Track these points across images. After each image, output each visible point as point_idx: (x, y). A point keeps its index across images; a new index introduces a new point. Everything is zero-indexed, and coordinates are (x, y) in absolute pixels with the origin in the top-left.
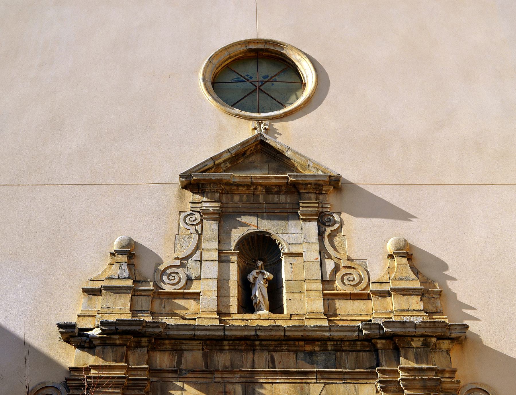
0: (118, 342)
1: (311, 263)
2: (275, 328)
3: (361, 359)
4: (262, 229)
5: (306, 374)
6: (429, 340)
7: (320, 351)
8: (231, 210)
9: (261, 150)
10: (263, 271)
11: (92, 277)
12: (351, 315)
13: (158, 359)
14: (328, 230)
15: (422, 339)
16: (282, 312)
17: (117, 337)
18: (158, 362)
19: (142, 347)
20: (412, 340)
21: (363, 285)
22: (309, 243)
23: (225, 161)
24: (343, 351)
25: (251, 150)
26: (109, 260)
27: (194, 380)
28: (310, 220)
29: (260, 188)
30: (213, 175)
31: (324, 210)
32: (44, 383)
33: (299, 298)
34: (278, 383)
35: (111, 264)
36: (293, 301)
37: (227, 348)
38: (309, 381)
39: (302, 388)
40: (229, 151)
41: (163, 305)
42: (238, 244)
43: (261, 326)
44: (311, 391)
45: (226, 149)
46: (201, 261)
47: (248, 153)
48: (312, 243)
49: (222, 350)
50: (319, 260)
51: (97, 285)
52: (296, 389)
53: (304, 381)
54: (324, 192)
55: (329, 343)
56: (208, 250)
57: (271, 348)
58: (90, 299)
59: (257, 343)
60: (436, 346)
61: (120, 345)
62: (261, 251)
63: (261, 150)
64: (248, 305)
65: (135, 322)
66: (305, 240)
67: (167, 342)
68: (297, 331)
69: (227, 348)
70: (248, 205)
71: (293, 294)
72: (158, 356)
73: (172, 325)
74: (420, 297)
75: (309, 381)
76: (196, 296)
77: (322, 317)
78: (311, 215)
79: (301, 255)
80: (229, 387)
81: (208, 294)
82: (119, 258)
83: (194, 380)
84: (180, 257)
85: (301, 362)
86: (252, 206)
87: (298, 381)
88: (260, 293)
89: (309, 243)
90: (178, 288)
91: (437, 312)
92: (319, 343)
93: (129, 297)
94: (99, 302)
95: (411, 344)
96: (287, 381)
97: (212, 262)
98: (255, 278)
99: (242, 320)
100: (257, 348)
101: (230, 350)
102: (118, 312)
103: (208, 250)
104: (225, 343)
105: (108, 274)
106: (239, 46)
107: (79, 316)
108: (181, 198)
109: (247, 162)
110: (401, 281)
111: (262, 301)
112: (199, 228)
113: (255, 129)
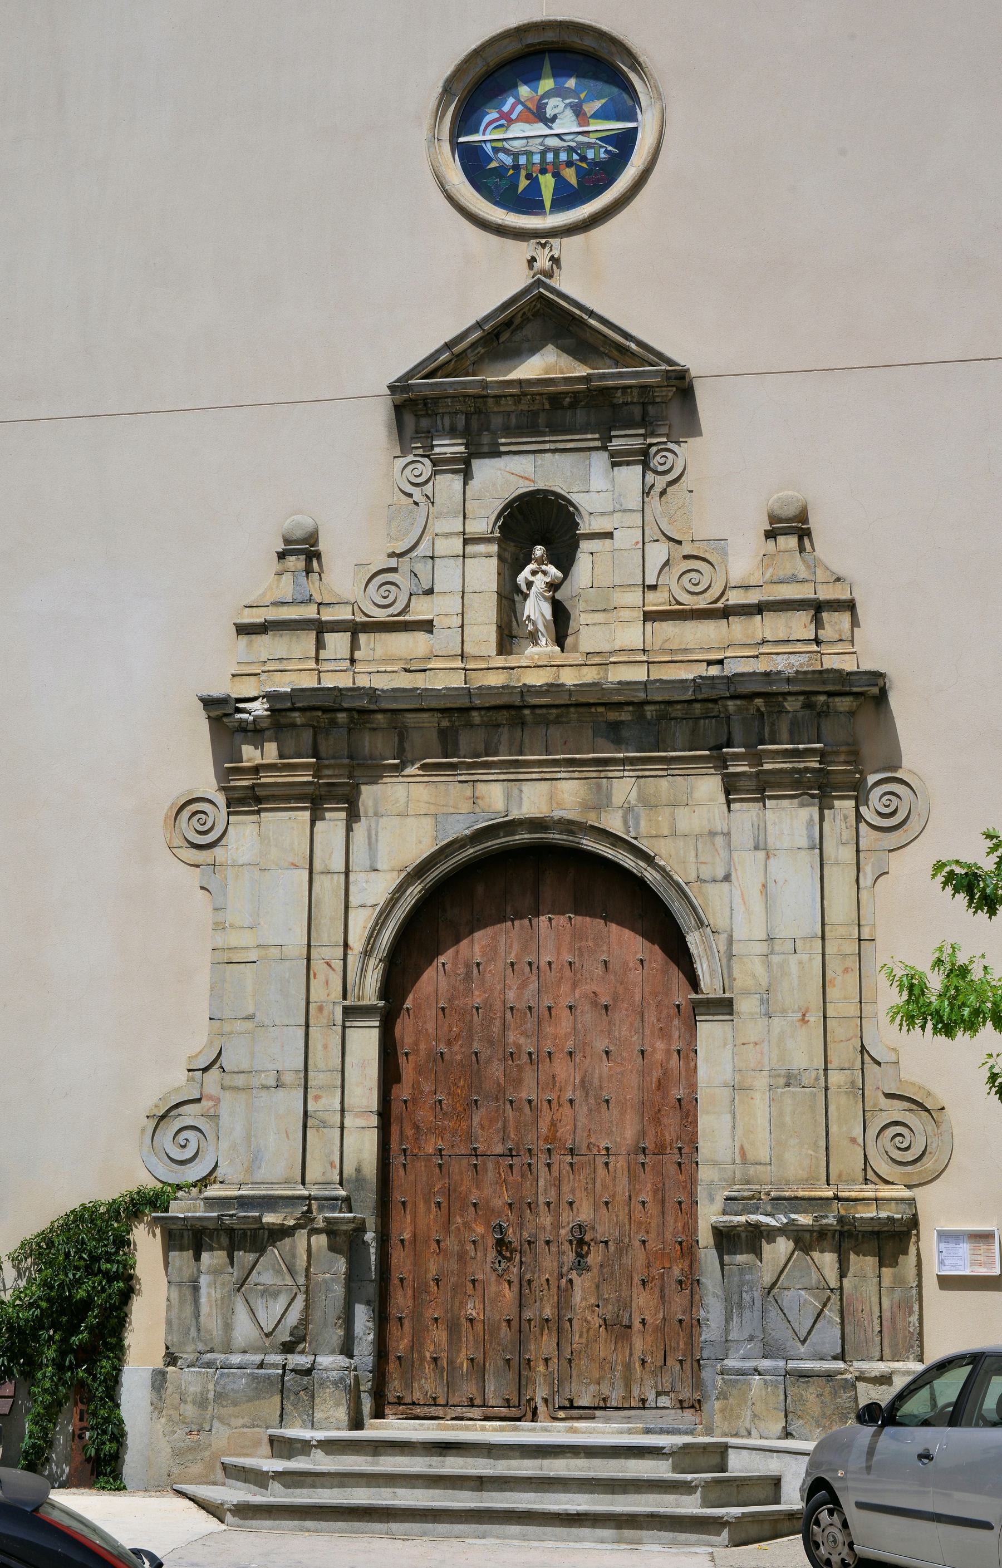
1: (626, 553)
2: (553, 689)
3: (702, 730)
4: (541, 485)
5: (606, 762)
6: (814, 699)
9: (541, 316)
10: (544, 567)
11: (248, 602)
12: (685, 651)
13: (367, 744)
15: (801, 698)
17: (296, 714)
18: (367, 749)
20: (785, 700)
21: (715, 592)
22: (624, 511)
23: (473, 345)
24: (671, 719)
25: (524, 313)
26: (275, 565)
27: (426, 779)
28: (628, 463)
32: (190, 792)
33: (603, 621)
34: (560, 779)
35: (279, 574)
36: (591, 627)
38: (610, 774)
39: (599, 787)
40: (479, 325)
41: (372, 646)
42: (584, 361)
43: (530, 686)
44: (614, 791)
45: (473, 322)
46: (432, 558)
47: (517, 321)
48: (630, 511)
50: (640, 545)
51: (256, 617)
52: (590, 789)
53: (603, 774)
54: (658, 400)
55: (648, 708)
56: (447, 535)
58: (250, 644)
59: (527, 712)
60: (828, 707)
62: (539, 527)
63: (541, 316)
64: (509, 635)
65: (321, 693)
71: (592, 615)
72: (367, 739)
73: (382, 690)
74: (812, 612)
75: (610, 774)
76: (427, 626)
77: (638, 659)
79: (609, 535)
81: (447, 622)
82: (291, 564)
84: (397, 552)
85: (600, 741)
87: (594, 775)
88: (536, 609)
89: (624, 511)
90: (396, 613)
91: (841, 640)
92: (631, 708)
93: (313, 635)
94: (266, 646)
95: (784, 707)
96: (576, 775)
97: (452, 560)
99: (503, 668)
102: (296, 668)
103: (447, 535)
104: (475, 714)
105: (278, 595)
106: (506, 42)
107: (233, 676)
109: (518, 337)
110: (781, 585)
112: (428, 489)
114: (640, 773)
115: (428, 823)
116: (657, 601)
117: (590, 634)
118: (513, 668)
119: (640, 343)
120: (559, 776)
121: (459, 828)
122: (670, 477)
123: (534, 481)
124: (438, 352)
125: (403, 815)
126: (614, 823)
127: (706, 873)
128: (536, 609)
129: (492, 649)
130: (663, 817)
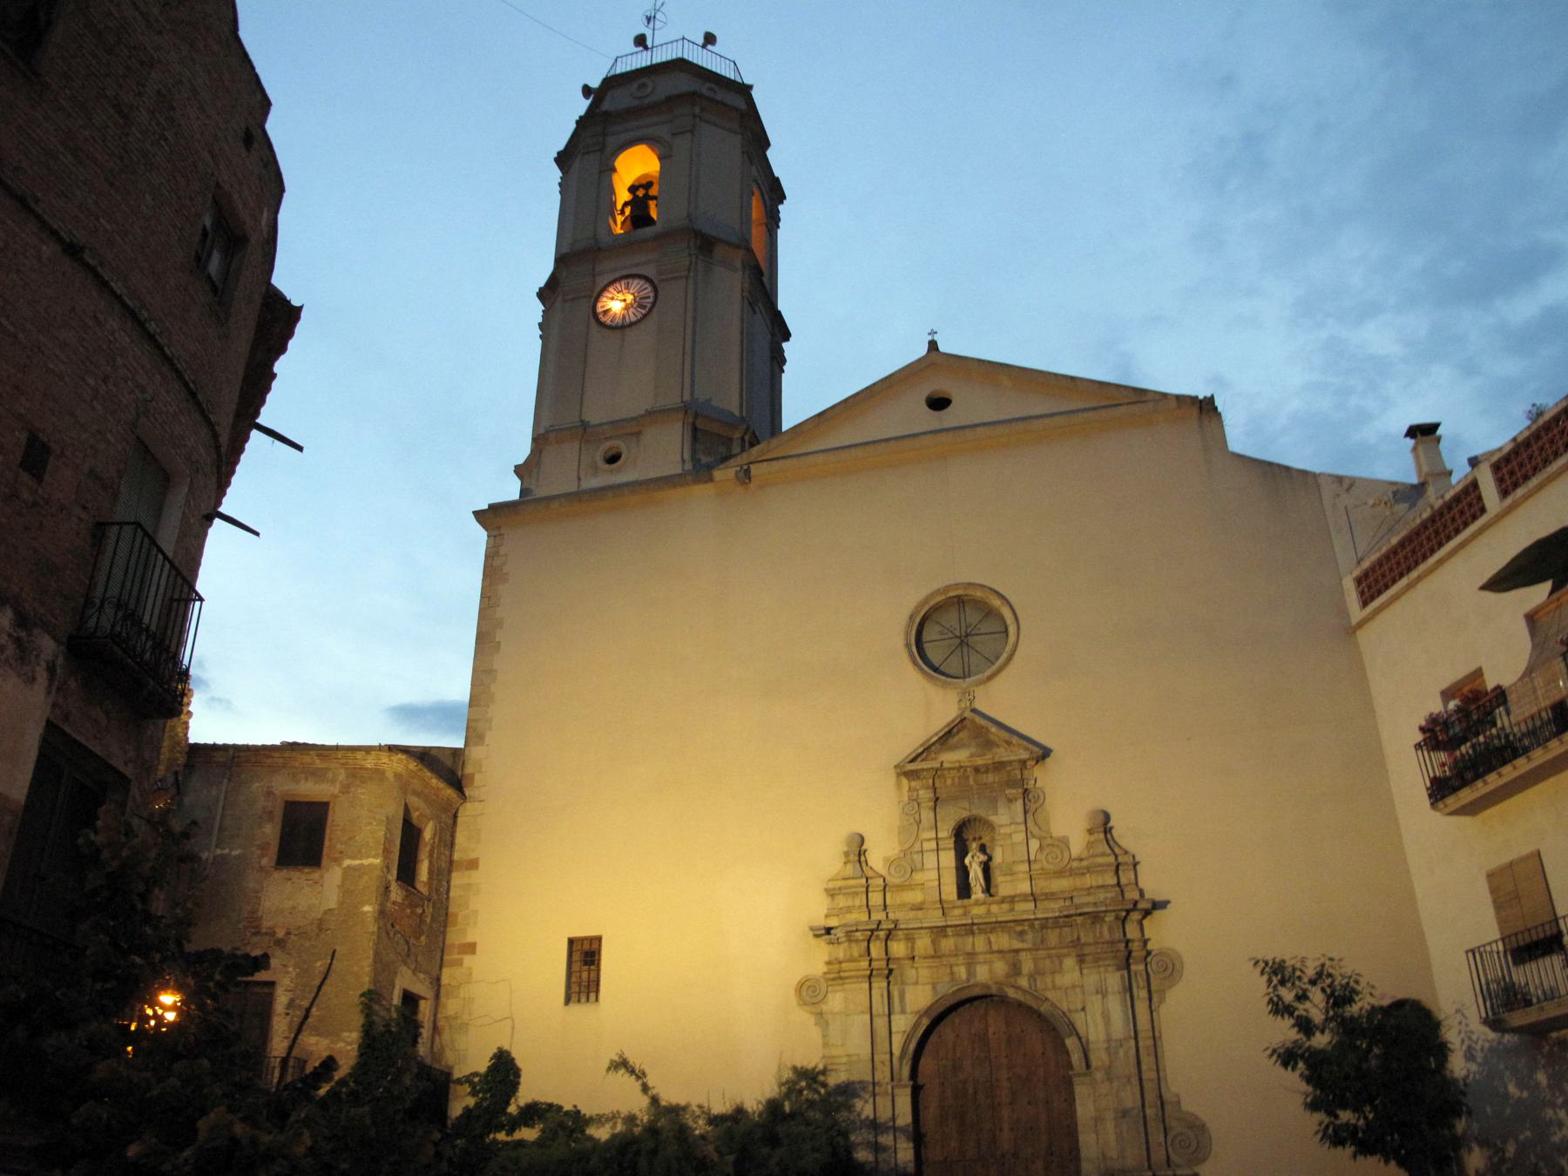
64: (964, 890)
80: (956, 969)
88: (975, 872)
108: (899, 785)
115: (929, 988)
117: (1004, 887)
121: (946, 988)
125: (916, 983)
126: (1023, 982)
127: (1072, 1007)
128: (975, 872)
130: (1048, 980)
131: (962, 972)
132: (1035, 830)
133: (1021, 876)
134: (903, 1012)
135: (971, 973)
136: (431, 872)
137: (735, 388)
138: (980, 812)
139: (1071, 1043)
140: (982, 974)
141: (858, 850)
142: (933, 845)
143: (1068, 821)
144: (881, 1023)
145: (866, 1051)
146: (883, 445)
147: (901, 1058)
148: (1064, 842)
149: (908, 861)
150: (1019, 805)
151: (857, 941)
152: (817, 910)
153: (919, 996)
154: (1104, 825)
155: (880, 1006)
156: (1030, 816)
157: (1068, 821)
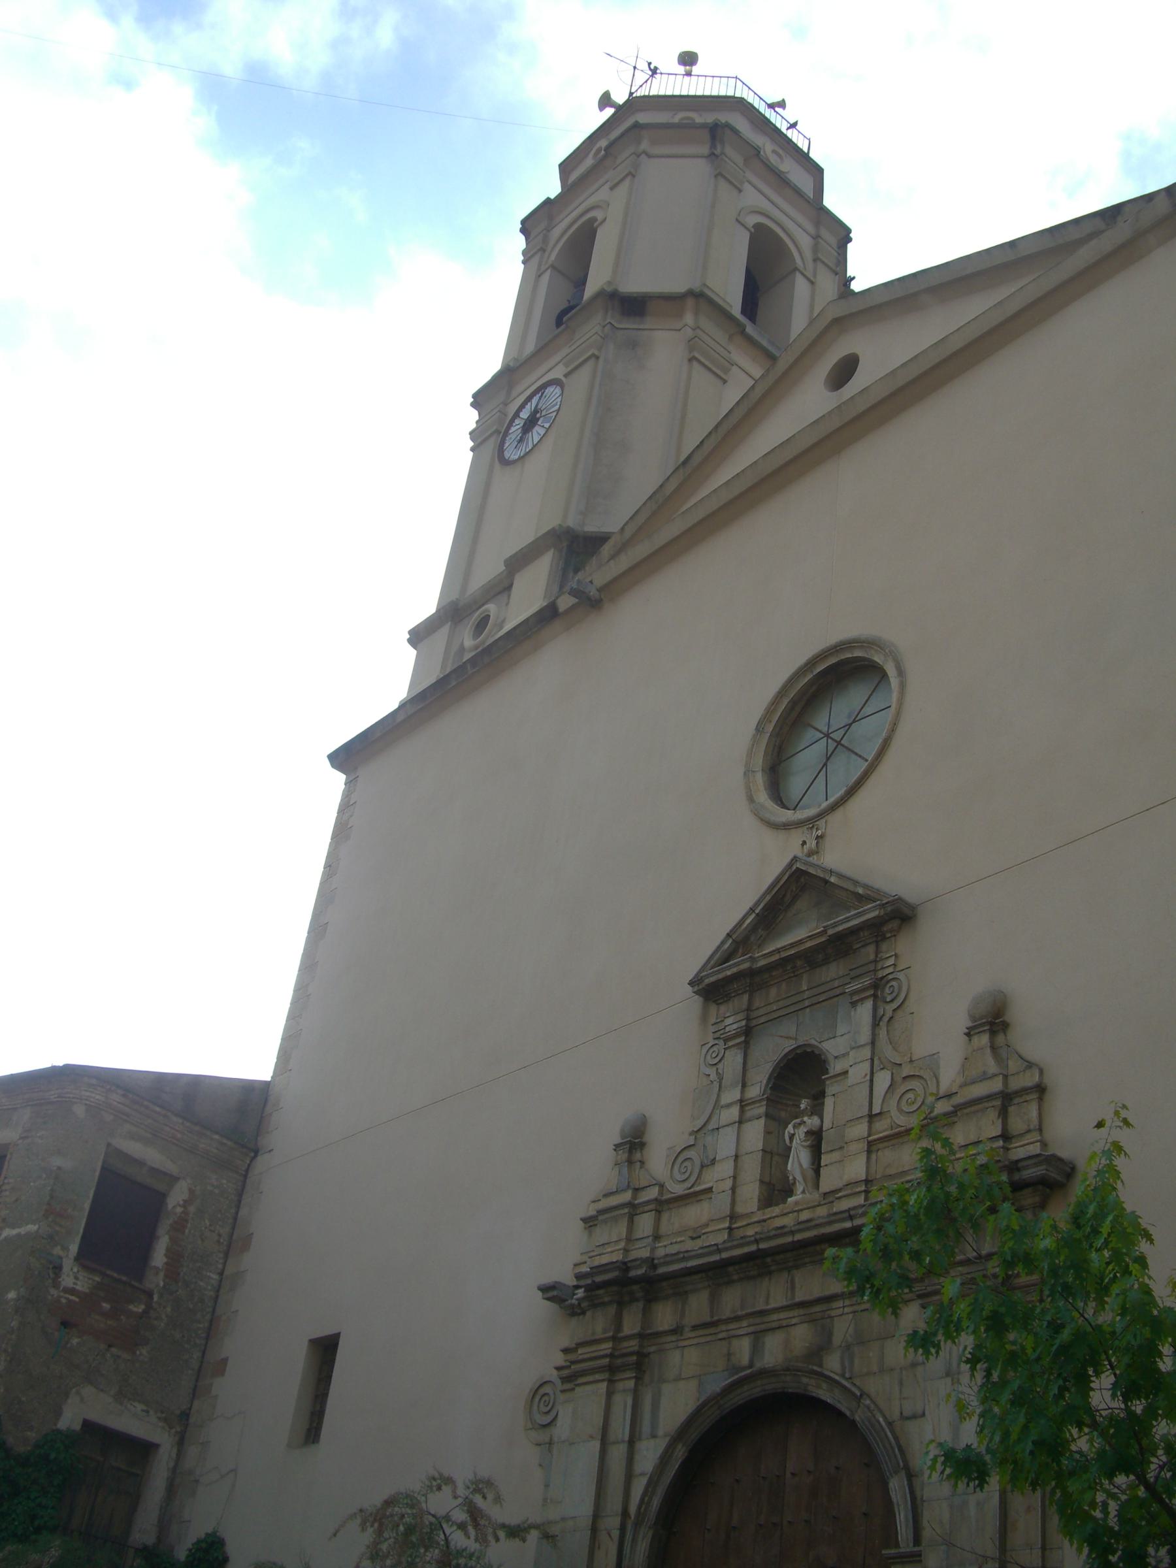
0: (606, 1299)
7: (646, 1311)
8: (762, 1020)
9: (798, 886)
14: (889, 1008)
16: (143, 1450)
17: (601, 1292)
19: (637, 1300)
29: (799, 963)
30: (740, 964)
31: (880, 974)
37: (735, 1277)
49: (730, 1282)
54: (888, 935)
57: (790, 1264)
61: (610, 1302)
66: (853, 1044)
67: (664, 1284)
68: (808, 1229)
69: (735, 1277)
70: (781, 1004)
78: (864, 990)
83: (695, 1341)
86: (789, 1001)
98: (792, 1137)
100: (773, 1268)
101: (741, 1280)
104: (731, 1269)
111: (799, 1177)
113: (804, 843)
114: (758, 1328)
116: (882, 1128)
118: (764, 1221)
119: (866, 886)
120: (794, 1321)
121: (715, 1385)
122: (895, 1005)
123: (796, 1039)
124: (723, 943)
125: (678, 1379)
129: (755, 1209)
131: (743, 1349)
132: (888, 1053)
133: (854, 1147)
134: (654, 1436)
135: (757, 1348)
136: (169, 1252)
137: (83, 1225)
138: (810, 1037)
139: (897, 1486)
140: (774, 1352)
141: (633, 1143)
142: (735, 1112)
143: (937, 1029)
144: (618, 1453)
145: (585, 1509)
146: (599, 1421)
147: (637, 1524)
148: (933, 1060)
149: (695, 1150)
150: (865, 1011)
151: (604, 1304)
152: (565, 1254)
153: (677, 1401)
154: (993, 1021)
155: (620, 1428)
156: (882, 1033)
157: (937, 1029)
